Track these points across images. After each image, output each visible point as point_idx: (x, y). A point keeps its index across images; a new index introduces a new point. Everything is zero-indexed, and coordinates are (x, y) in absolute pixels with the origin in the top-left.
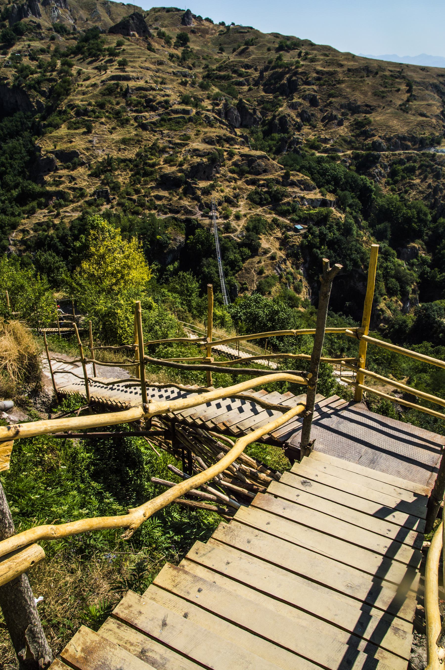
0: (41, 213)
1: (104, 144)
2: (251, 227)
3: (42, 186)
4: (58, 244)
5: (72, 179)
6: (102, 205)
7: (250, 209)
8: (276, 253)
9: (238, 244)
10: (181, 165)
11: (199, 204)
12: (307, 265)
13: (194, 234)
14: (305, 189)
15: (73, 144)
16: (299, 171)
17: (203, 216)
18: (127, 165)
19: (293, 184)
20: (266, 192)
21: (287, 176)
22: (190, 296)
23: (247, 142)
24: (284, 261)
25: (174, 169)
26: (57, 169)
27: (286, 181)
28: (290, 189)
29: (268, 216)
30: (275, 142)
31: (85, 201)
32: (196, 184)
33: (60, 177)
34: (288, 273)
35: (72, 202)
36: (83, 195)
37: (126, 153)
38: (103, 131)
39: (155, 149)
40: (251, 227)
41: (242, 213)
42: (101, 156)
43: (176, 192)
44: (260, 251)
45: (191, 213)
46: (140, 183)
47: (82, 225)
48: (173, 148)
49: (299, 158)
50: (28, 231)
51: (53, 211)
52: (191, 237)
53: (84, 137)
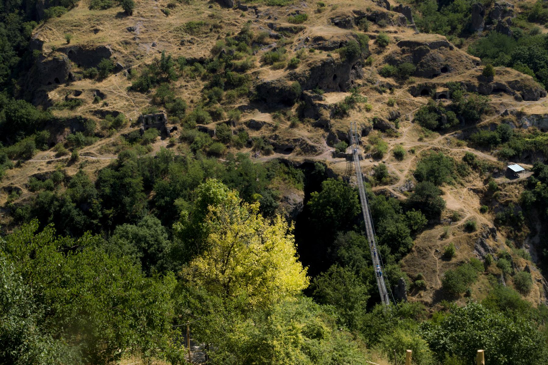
0: (43, 158)
1: (155, 34)
2: (424, 172)
3: (45, 109)
4: (75, 212)
5: (100, 95)
6: (153, 141)
7: (420, 140)
8: (474, 218)
9: (401, 204)
10: (292, 66)
11: (327, 134)
12: (537, 239)
13: (320, 190)
14: (524, 98)
15: (100, 34)
16: (510, 65)
17: (335, 155)
18: (196, 70)
19: (499, 90)
20: (449, 108)
21: (487, 75)
22: (351, 308)
23: (410, 18)
24: (492, 233)
25: (281, 74)
26: (71, 79)
27: (486, 85)
28: (494, 100)
29: (455, 150)
30: (460, 16)
31: (124, 136)
32: (321, 99)
33: (78, 93)
34: (501, 256)
35: (99, 136)
36: (118, 125)
37: (195, 47)
38: (152, 11)
39: (244, 40)
40: (424, 172)
41: (407, 147)
42: (150, 55)
43: (285, 114)
44: (445, 215)
45: (312, 150)
46: (219, 100)
47: (118, 178)
48: (277, 37)
49: (508, 40)
50: (18, 190)
51: (64, 154)
52: (315, 194)
53: (119, 21)
